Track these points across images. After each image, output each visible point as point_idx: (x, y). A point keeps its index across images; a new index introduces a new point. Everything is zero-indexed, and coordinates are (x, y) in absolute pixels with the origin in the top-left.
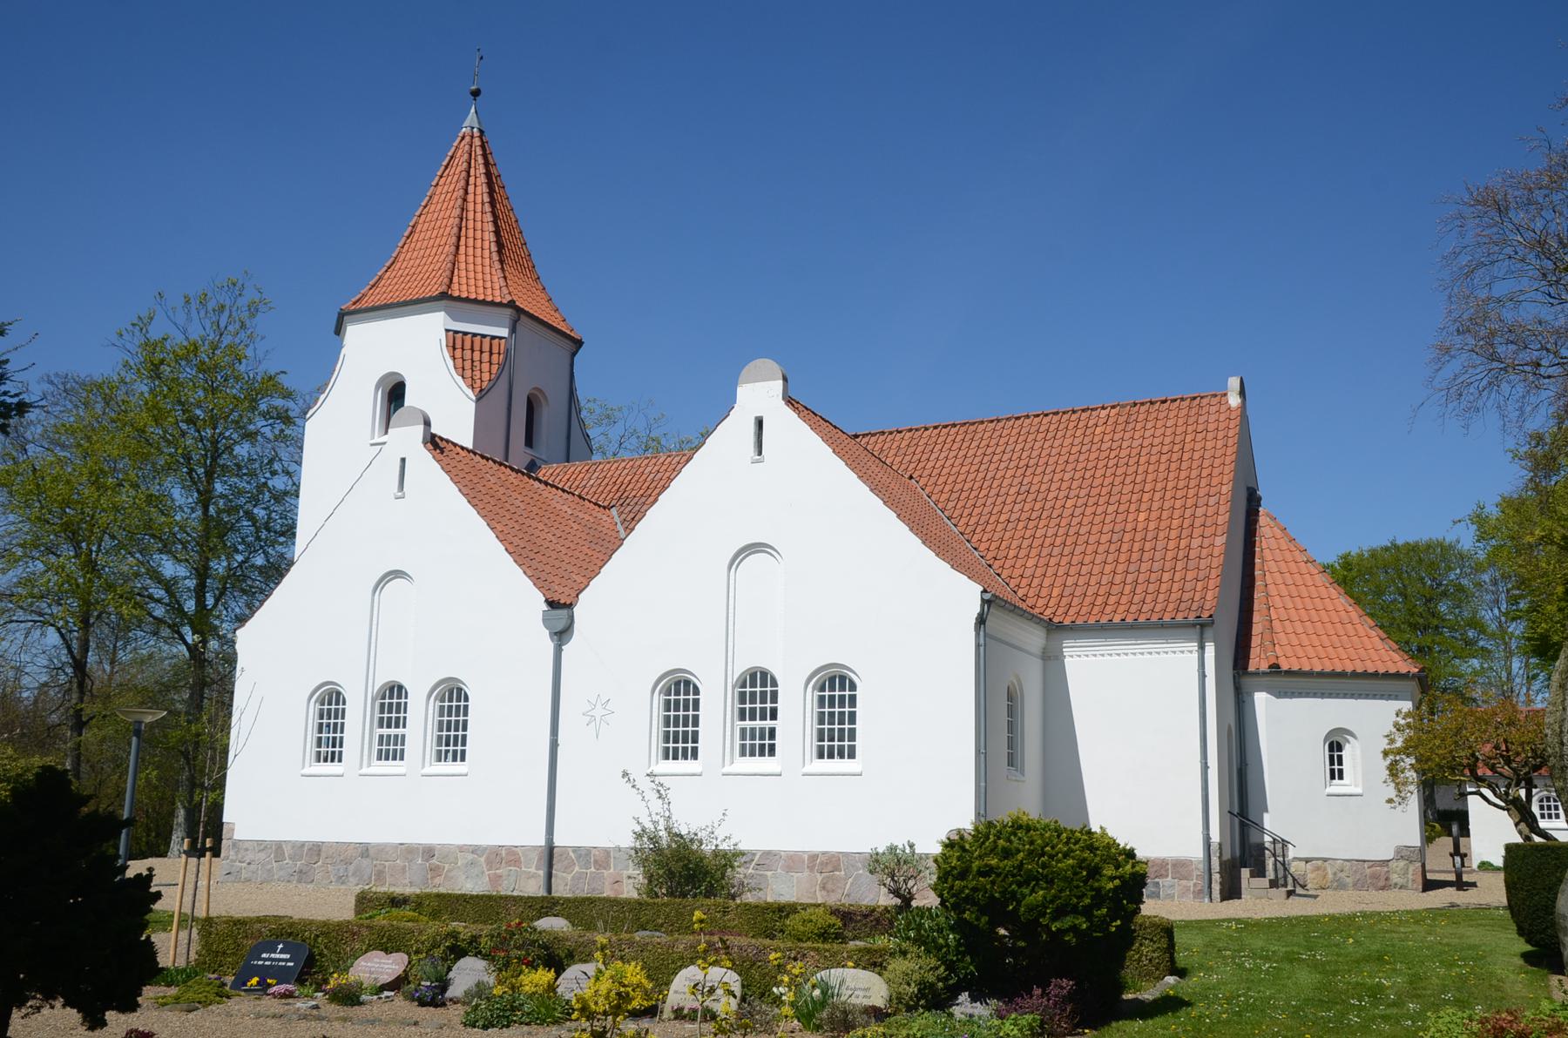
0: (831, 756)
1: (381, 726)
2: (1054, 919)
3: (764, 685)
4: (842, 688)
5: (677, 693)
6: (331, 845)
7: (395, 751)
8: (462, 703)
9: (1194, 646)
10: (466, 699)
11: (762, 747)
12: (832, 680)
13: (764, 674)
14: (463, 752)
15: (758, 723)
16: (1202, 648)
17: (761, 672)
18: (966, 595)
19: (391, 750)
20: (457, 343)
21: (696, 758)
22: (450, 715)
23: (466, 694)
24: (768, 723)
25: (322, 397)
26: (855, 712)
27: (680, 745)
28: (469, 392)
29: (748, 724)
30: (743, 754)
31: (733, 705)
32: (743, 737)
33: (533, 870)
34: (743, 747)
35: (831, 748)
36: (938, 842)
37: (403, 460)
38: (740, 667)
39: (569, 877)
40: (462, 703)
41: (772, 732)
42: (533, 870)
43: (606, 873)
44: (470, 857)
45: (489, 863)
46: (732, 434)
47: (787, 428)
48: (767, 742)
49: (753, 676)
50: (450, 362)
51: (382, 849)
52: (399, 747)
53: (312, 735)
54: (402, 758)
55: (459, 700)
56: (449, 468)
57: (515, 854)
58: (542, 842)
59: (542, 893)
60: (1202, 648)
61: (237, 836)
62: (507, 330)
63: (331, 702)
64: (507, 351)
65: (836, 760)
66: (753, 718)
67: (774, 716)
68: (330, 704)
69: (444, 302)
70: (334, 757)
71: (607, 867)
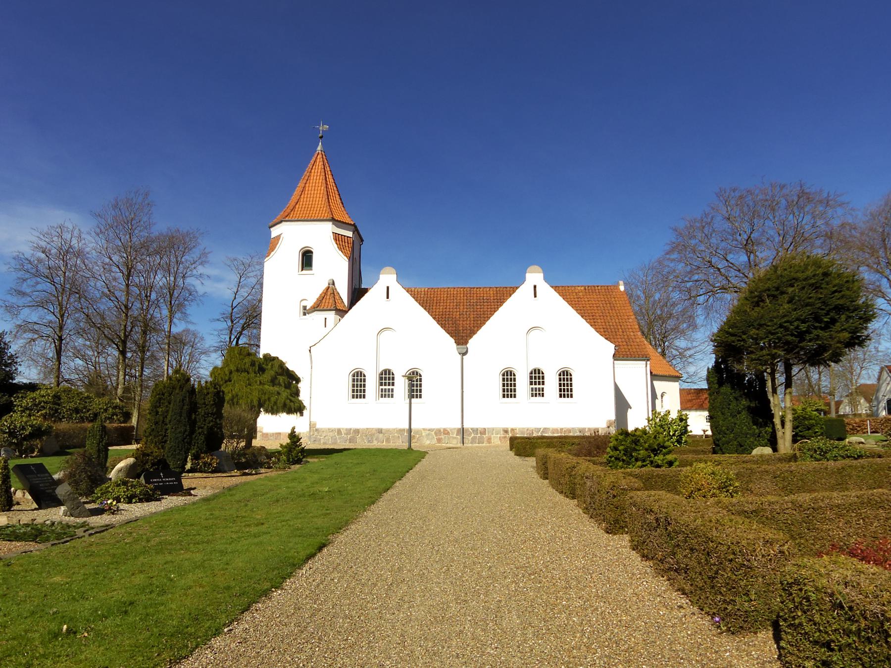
0: (357, 398)
6: (363, 429)
12: (507, 372)
13: (389, 371)
15: (537, 386)
19: (538, 393)
20: (337, 237)
24: (541, 386)
27: (359, 394)
28: (346, 258)
29: (534, 386)
30: (382, 397)
32: (382, 391)
33: (455, 436)
34: (382, 395)
35: (357, 395)
36: (294, 428)
39: (470, 438)
42: (455, 436)
43: (484, 436)
44: (428, 432)
45: (436, 434)
46: (525, 290)
47: (545, 290)
49: (535, 370)
50: (336, 245)
51: (388, 430)
53: (351, 388)
56: (508, 295)
57: (446, 430)
58: (407, 427)
59: (405, 446)
61: (265, 431)
62: (352, 233)
64: (353, 241)
67: (543, 383)
71: (485, 434)
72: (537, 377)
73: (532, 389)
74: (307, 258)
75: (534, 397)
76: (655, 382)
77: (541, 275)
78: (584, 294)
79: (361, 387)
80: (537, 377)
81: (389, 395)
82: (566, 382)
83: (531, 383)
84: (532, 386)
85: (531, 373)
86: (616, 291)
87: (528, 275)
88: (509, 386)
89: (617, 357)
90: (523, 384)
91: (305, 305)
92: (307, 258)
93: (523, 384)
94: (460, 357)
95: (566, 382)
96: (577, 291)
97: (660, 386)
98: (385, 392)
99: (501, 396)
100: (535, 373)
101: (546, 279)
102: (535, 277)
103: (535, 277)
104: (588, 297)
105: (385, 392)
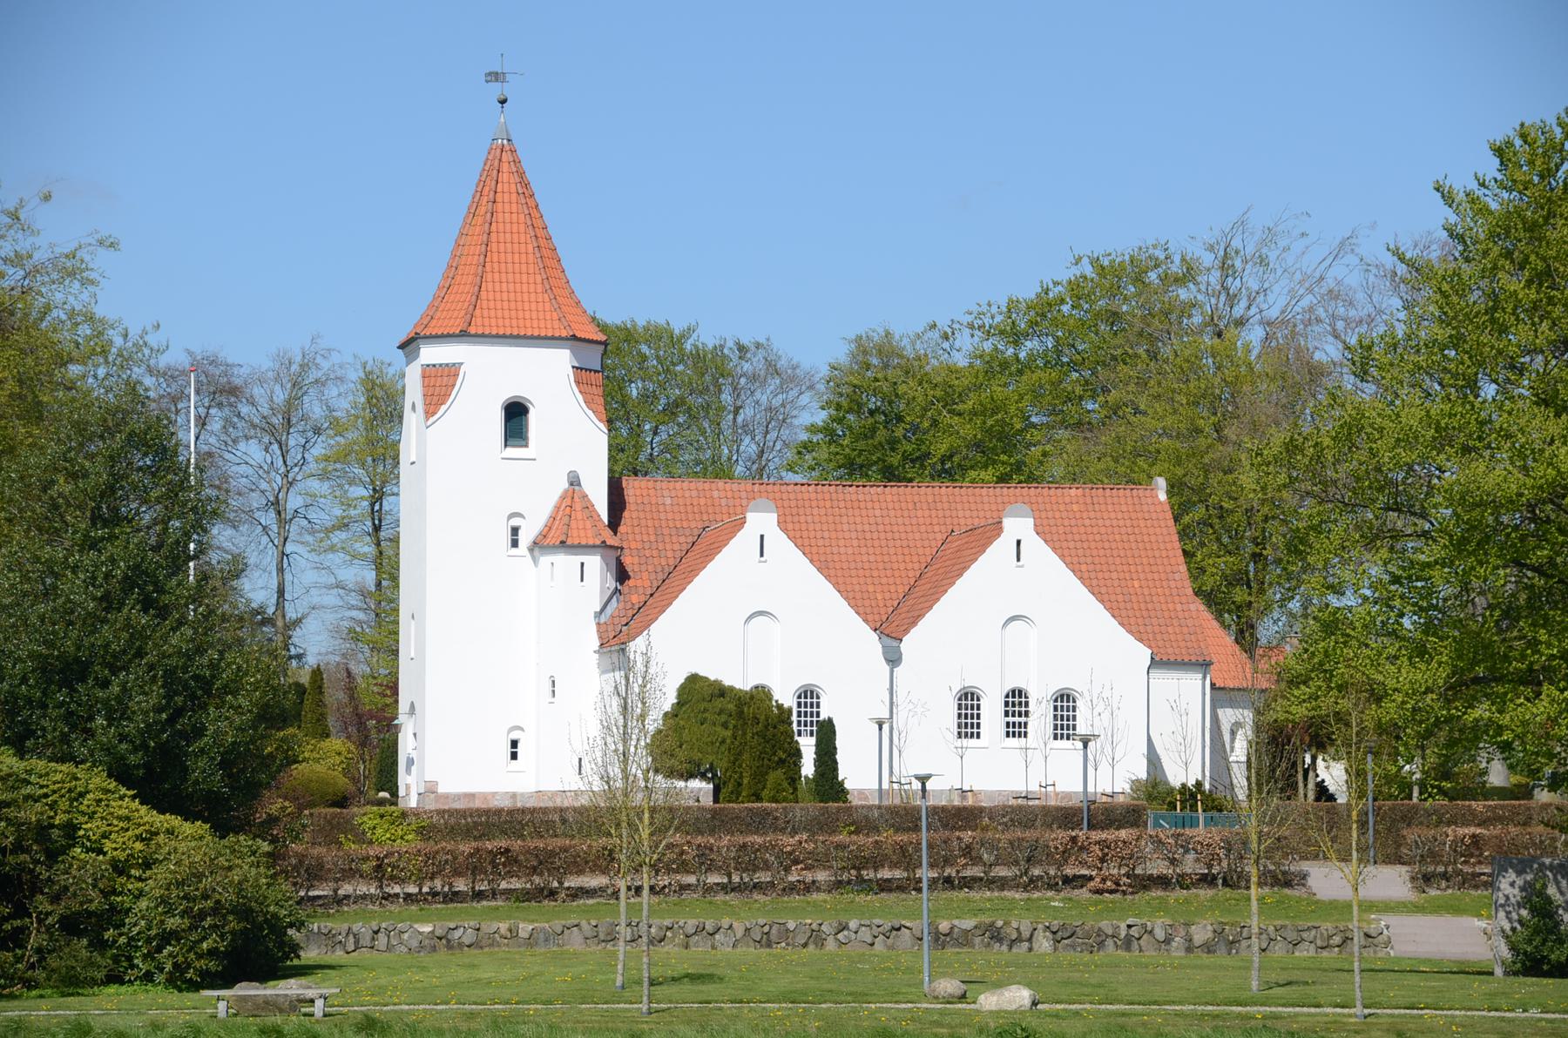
2: (1091, 878)
3: (1020, 697)
4: (1068, 701)
5: (806, 697)
9: (1200, 676)
10: (818, 697)
11: (972, 733)
15: (1017, 719)
16: (1204, 678)
18: (1144, 654)
19: (1016, 730)
24: (1023, 719)
25: (443, 408)
29: (1010, 719)
31: (1001, 708)
37: (762, 537)
38: (1008, 687)
49: (1014, 692)
60: (1204, 678)
63: (968, 702)
66: (1013, 716)
69: (569, 343)
72: (1016, 701)
73: (1008, 724)
74: (516, 413)
75: (1011, 739)
76: (1220, 712)
77: (773, 517)
78: (1082, 508)
79: (812, 716)
80: (1016, 701)
81: (1020, 733)
82: (969, 712)
83: (1007, 714)
84: (1007, 719)
85: (1007, 696)
86: (1149, 501)
87: (750, 516)
88: (968, 720)
89: (1156, 663)
90: (992, 714)
91: (514, 550)
92: (516, 413)
93: (992, 714)
94: (887, 668)
95: (1065, 713)
96: (1067, 500)
97: (1228, 716)
98: (1014, 727)
99: (1004, 734)
100: (1014, 697)
101: (783, 525)
102: (762, 521)
103: (762, 521)
104: (1092, 515)
105: (1014, 727)
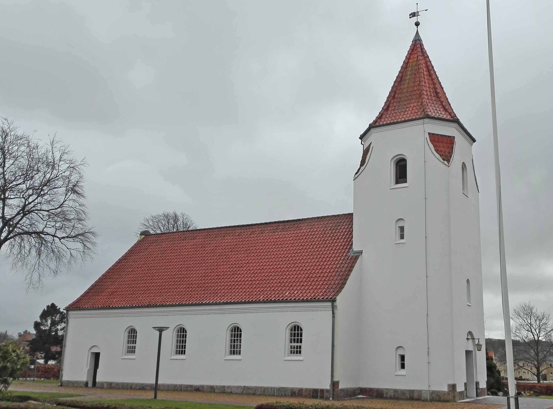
1: (291, 342)
7: (182, 351)
8: (184, 334)
10: (186, 332)
14: (135, 351)
17: (297, 326)
21: (240, 354)
22: (295, 336)
23: (240, 329)
24: (299, 344)
26: (302, 339)
29: (293, 344)
40: (184, 334)
41: (300, 347)
48: (298, 350)
52: (183, 349)
54: (184, 354)
55: (238, 332)
65: (232, 355)
67: (301, 342)
68: (181, 333)
70: (183, 352)
